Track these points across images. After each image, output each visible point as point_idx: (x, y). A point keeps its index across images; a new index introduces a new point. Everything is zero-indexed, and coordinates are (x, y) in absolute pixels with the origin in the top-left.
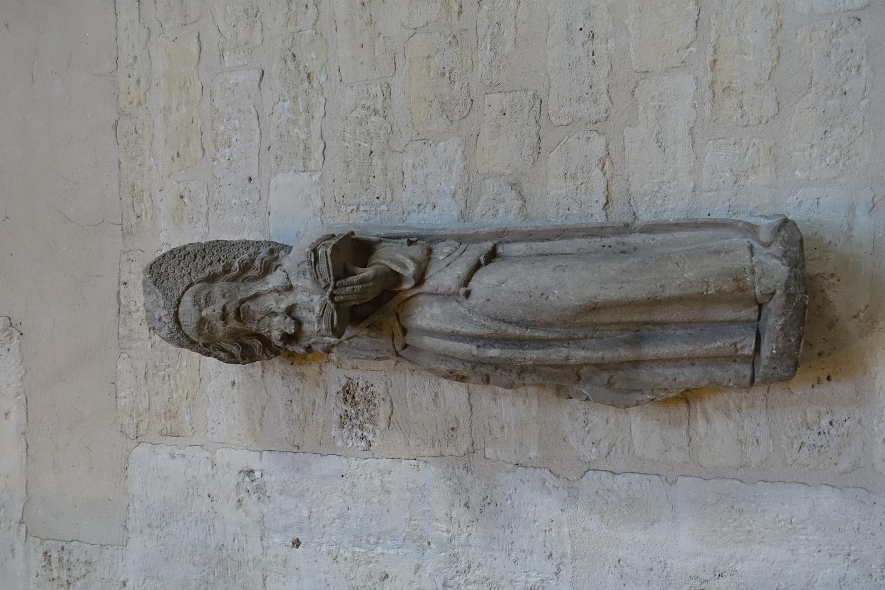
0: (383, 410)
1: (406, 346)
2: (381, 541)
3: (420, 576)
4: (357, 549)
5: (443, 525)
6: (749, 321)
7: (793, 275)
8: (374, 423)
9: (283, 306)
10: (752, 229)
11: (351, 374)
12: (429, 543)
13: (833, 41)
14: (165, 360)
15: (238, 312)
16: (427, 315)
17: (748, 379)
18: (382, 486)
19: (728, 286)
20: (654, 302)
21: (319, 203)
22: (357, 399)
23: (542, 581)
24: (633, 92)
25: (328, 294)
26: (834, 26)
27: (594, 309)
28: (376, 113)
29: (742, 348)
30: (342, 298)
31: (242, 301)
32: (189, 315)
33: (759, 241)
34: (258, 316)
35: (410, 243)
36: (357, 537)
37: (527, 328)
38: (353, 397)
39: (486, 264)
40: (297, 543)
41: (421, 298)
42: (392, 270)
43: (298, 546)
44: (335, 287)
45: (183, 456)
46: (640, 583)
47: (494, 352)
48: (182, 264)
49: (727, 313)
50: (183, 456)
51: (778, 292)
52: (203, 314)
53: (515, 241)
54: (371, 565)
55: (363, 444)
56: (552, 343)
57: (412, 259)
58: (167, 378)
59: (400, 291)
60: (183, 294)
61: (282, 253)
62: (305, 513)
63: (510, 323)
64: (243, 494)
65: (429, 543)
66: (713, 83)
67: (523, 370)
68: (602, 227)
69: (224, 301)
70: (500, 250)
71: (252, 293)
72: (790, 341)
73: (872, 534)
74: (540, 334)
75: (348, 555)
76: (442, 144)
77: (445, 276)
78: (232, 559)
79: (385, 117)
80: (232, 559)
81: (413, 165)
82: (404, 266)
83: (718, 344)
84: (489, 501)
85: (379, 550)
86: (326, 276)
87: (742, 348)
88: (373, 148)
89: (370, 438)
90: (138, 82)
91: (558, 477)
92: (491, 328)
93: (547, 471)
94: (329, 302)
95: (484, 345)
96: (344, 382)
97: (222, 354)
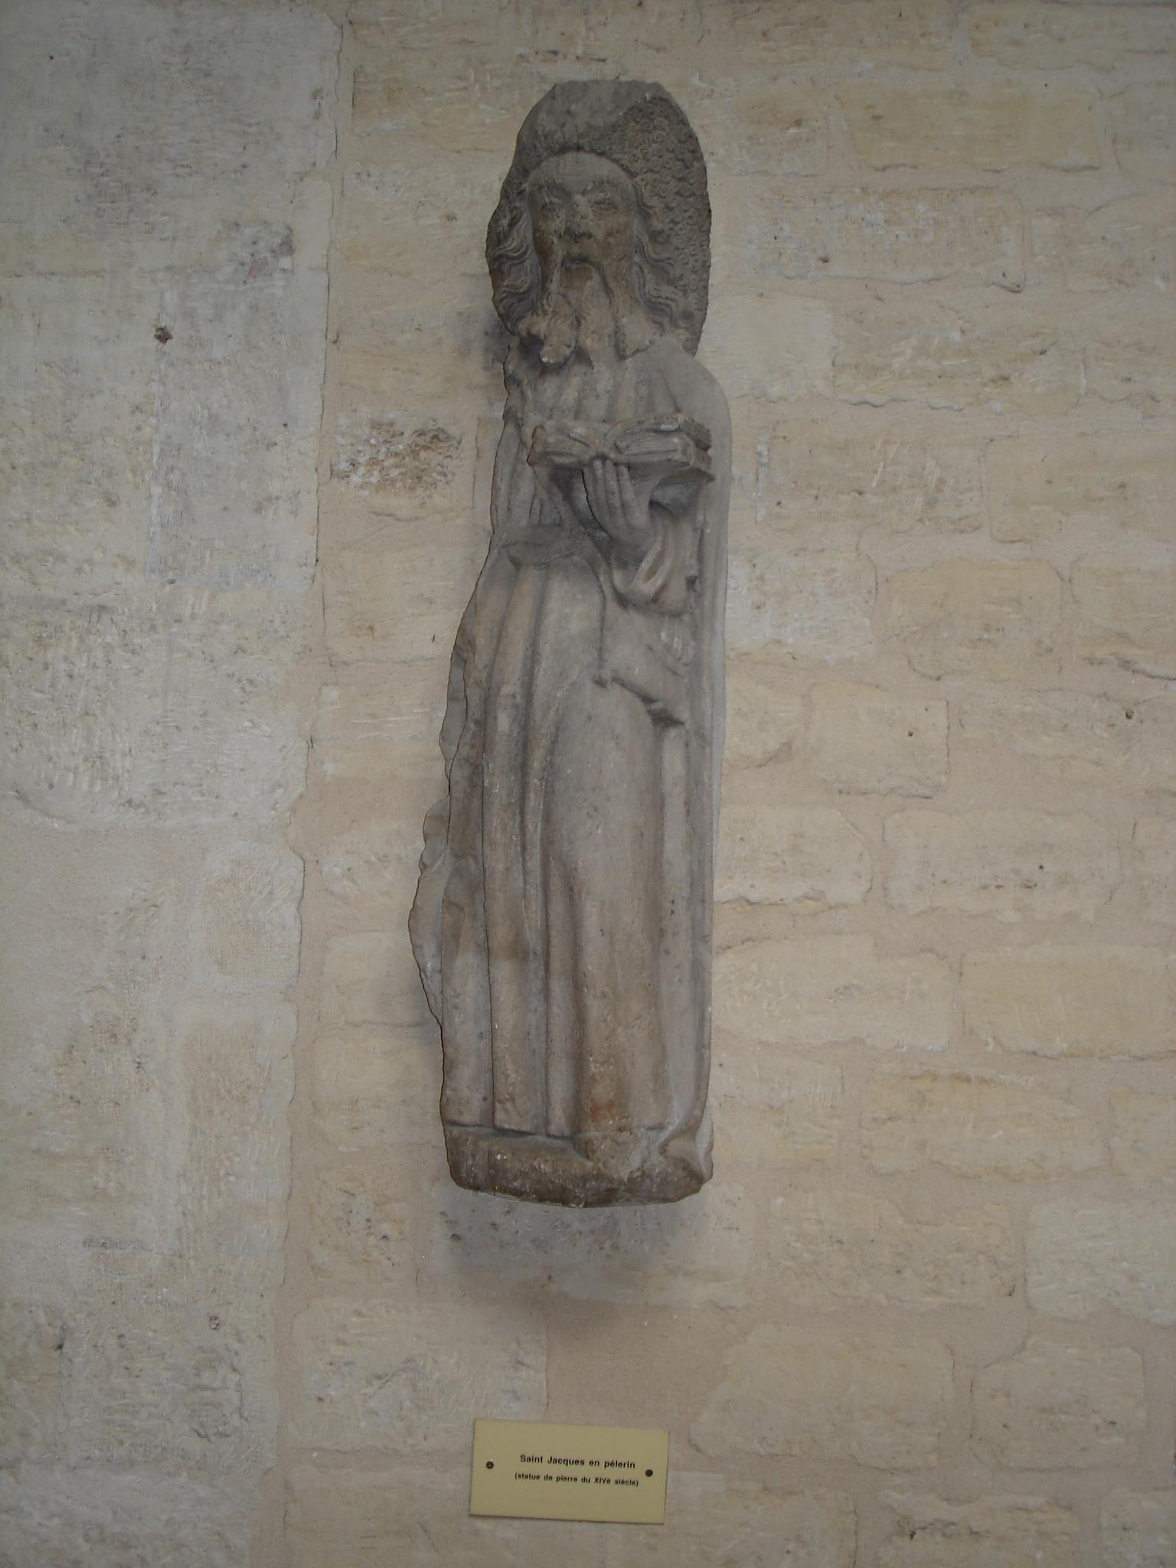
0: (401, 503)
1: (517, 564)
2: (173, 493)
3: (115, 565)
4: (156, 450)
5: (204, 608)
6: (547, 1121)
7: (615, 1186)
8: (380, 487)
9: (588, 343)
10: (690, 1129)
11: (468, 444)
12: (172, 582)
13: (981, 1258)
14: (496, 83)
15: (583, 259)
16: (570, 608)
17: (457, 1118)
18: (269, 499)
19: (601, 1092)
20: (577, 984)
21: (775, 391)
22: (423, 454)
23: (117, 778)
24: (931, 951)
25: (606, 450)
26: (1003, 1258)
27: (571, 889)
28: (931, 503)
29: (506, 1111)
30: (599, 472)
31: (599, 268)
32: (573, 169)
33: (673, 1136)
34: (573, 295)
35: (691, 582)
36: (179, 449)
37: (541, 779)
38: (425, 448)
39: (649, 712)
40: (163, 336)
41: (597, 599)
42: (645, 554)
43: (159, 337)
44: (616, 464)
45: (317, 115)
46: (122, 938)
47: (504, 722)
48: (668, 156)
49: (560, 1089)
50: (317, 115)
51: (590, 1164)
52: (578, 198)
53: (688, 759)
54: (130, 476)
55: (344, 466)
56: (518, 820)
57: (664, 587)
58: (462, 84)
59: (609, 565)
60: (616, 161)
61: (684, 335)
62: (218, 353)
63: (551, 752)
64: (248, 232)
65: (172, 582)
66: (935, 1077)
67: (477, 770)
68: (703, 901)
69: (600, 235)
70: (673, 732)
71: (612, 285)
72: (515, 1179)
73: (214, 1291)
74: (534, 801)
75: (147, 431)
76: (867, 622)
77: (632, 648)
78: (131, 210)
79: (920, 520)
80: (131, 210)
81: (834, 570)
82: (652, 573)
83: (513, 1076)
84: (249, 688)
85: (157, 491)
86: (634, 449)
87: (506, 1111)
88: (868, 496)
89: (356, 479)
90: (1016, 43)
91: (293, 810)
92: (544, 726)
93: (301, 790)
94: (593, 453)
95: (516, 707)
96: (453, 431)
97: (505, 222)
